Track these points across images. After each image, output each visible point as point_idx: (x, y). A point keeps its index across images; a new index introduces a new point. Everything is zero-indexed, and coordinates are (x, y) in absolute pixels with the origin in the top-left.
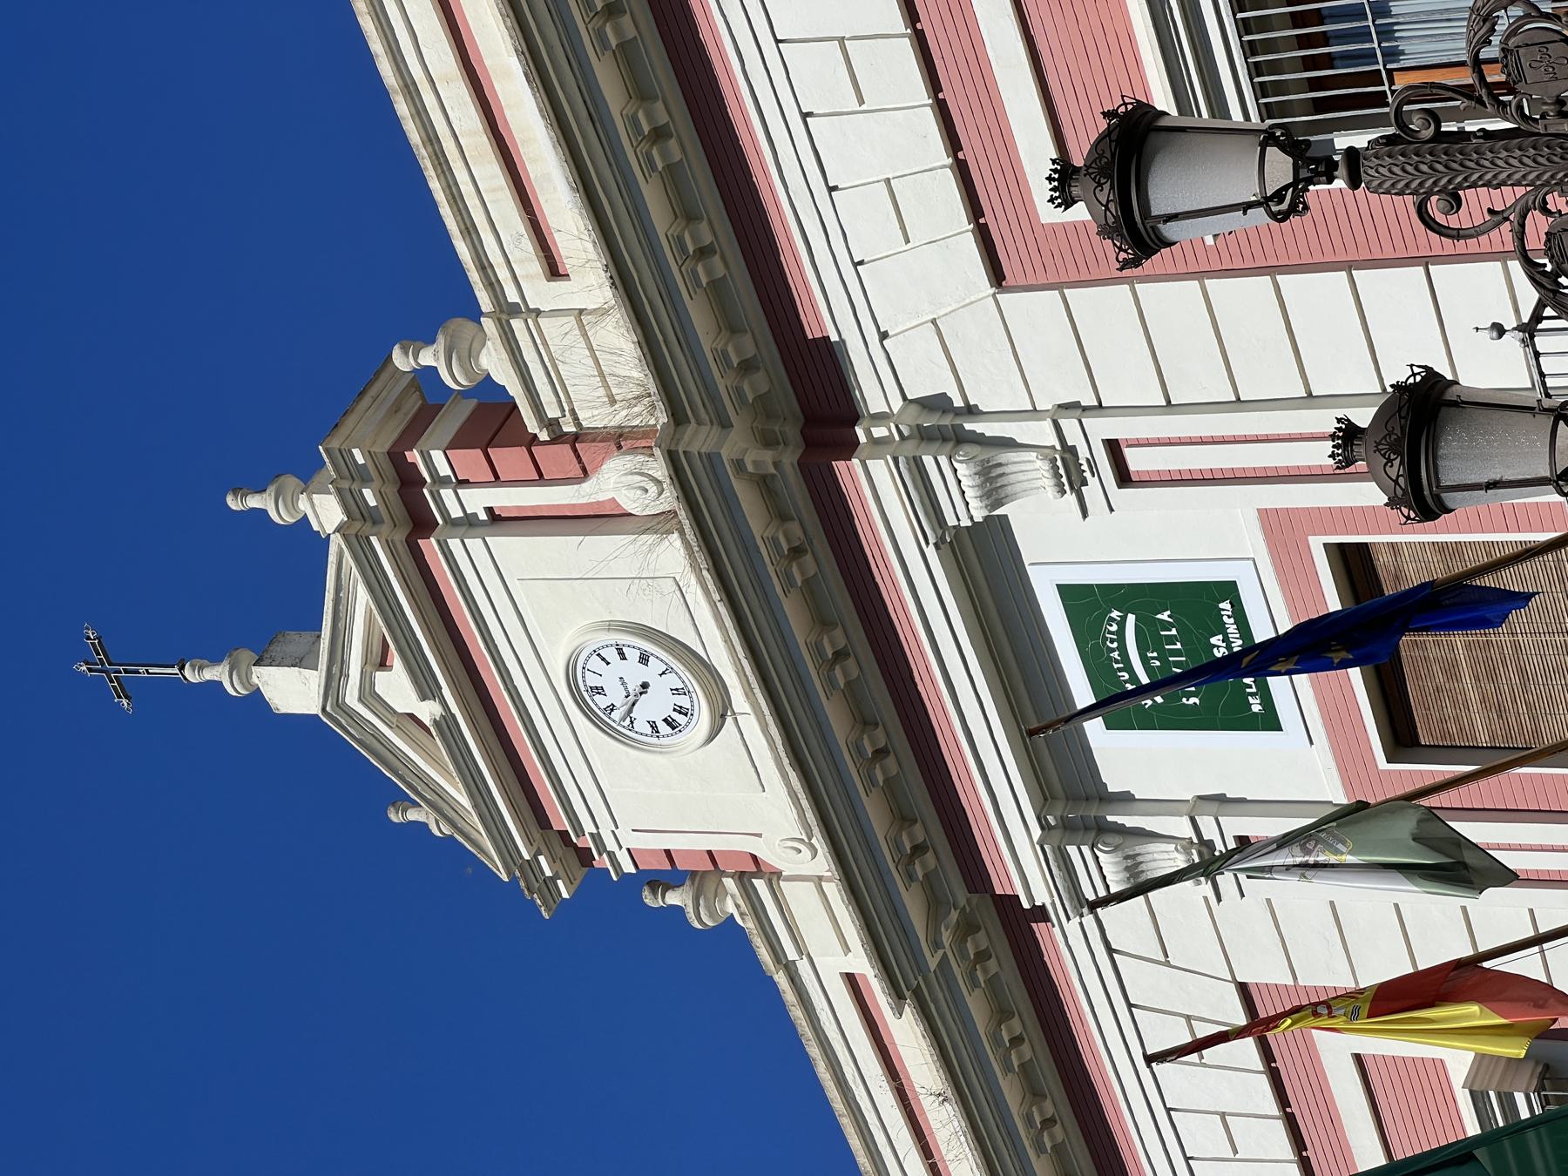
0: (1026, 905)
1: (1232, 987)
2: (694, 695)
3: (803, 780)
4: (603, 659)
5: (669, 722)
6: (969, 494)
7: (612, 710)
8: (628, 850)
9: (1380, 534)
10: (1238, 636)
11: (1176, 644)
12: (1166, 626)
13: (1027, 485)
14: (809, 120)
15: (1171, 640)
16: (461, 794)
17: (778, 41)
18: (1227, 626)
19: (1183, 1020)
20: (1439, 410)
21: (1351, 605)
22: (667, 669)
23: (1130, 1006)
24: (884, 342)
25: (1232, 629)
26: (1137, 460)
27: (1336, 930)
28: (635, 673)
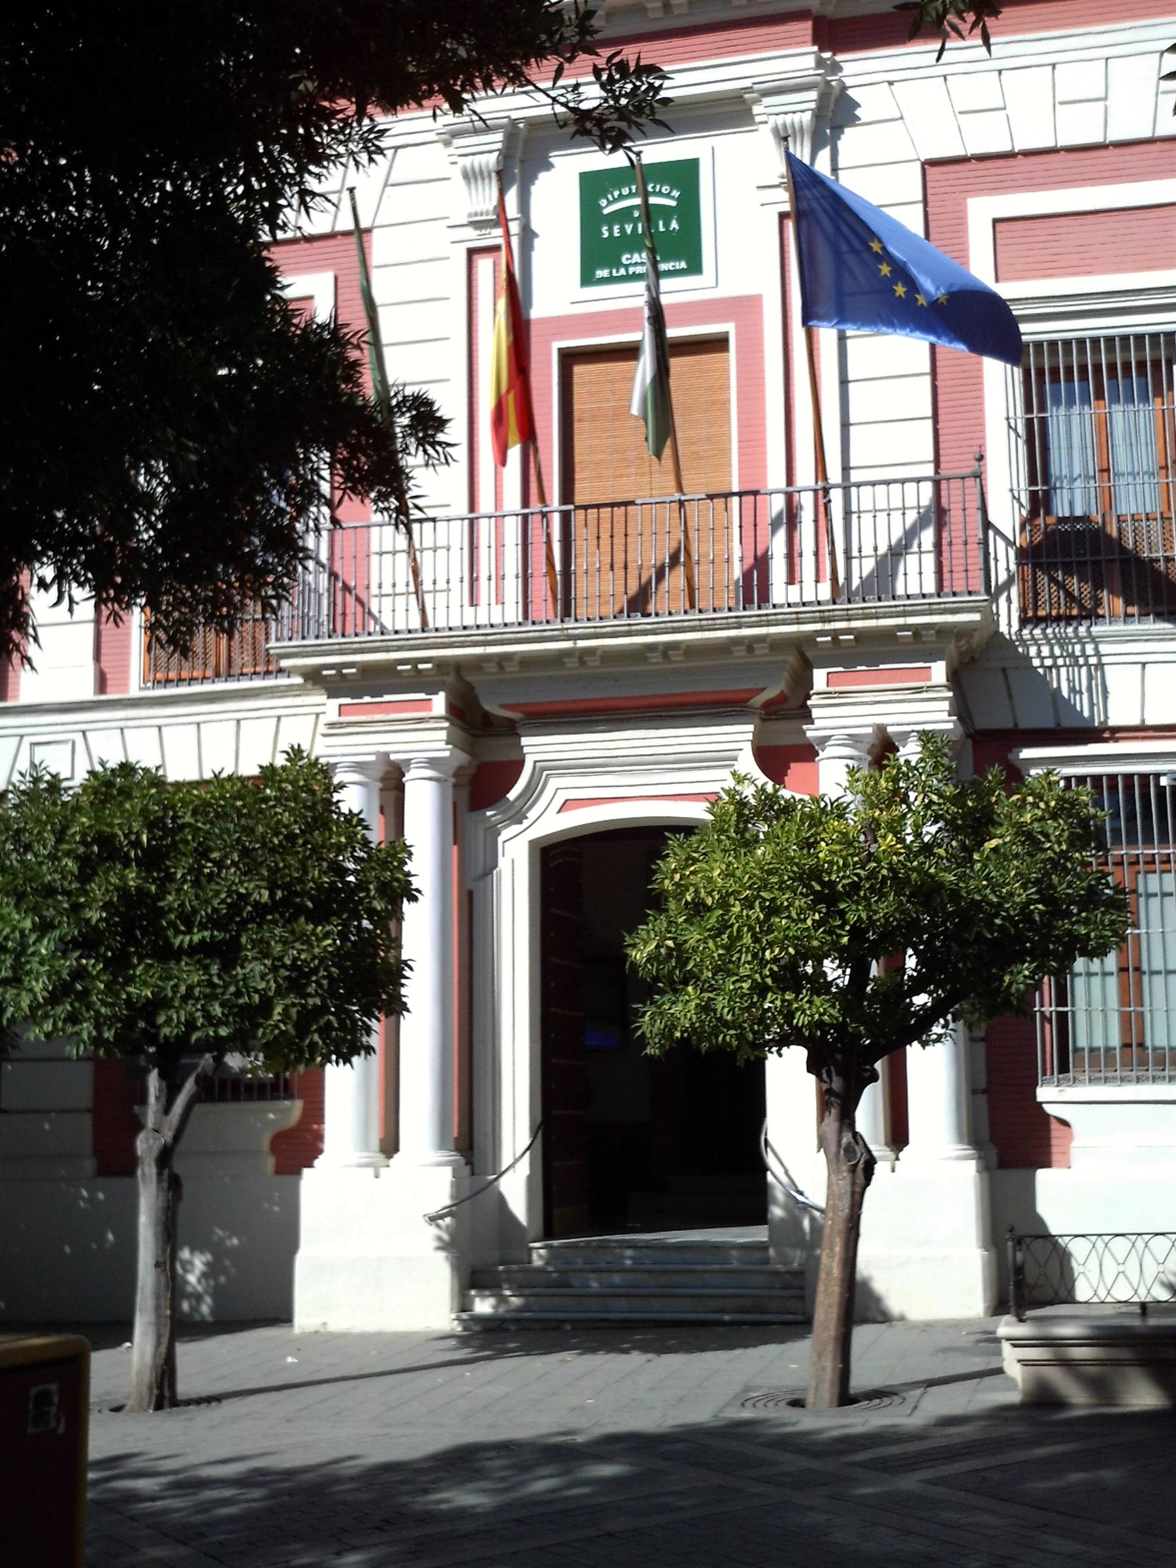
6: (788, 119)
13: (473, 189)
17: (1107, 59)
19: (388, 189)
20: (572, 369)
21: (1010, 756)
27: (325, 1386)
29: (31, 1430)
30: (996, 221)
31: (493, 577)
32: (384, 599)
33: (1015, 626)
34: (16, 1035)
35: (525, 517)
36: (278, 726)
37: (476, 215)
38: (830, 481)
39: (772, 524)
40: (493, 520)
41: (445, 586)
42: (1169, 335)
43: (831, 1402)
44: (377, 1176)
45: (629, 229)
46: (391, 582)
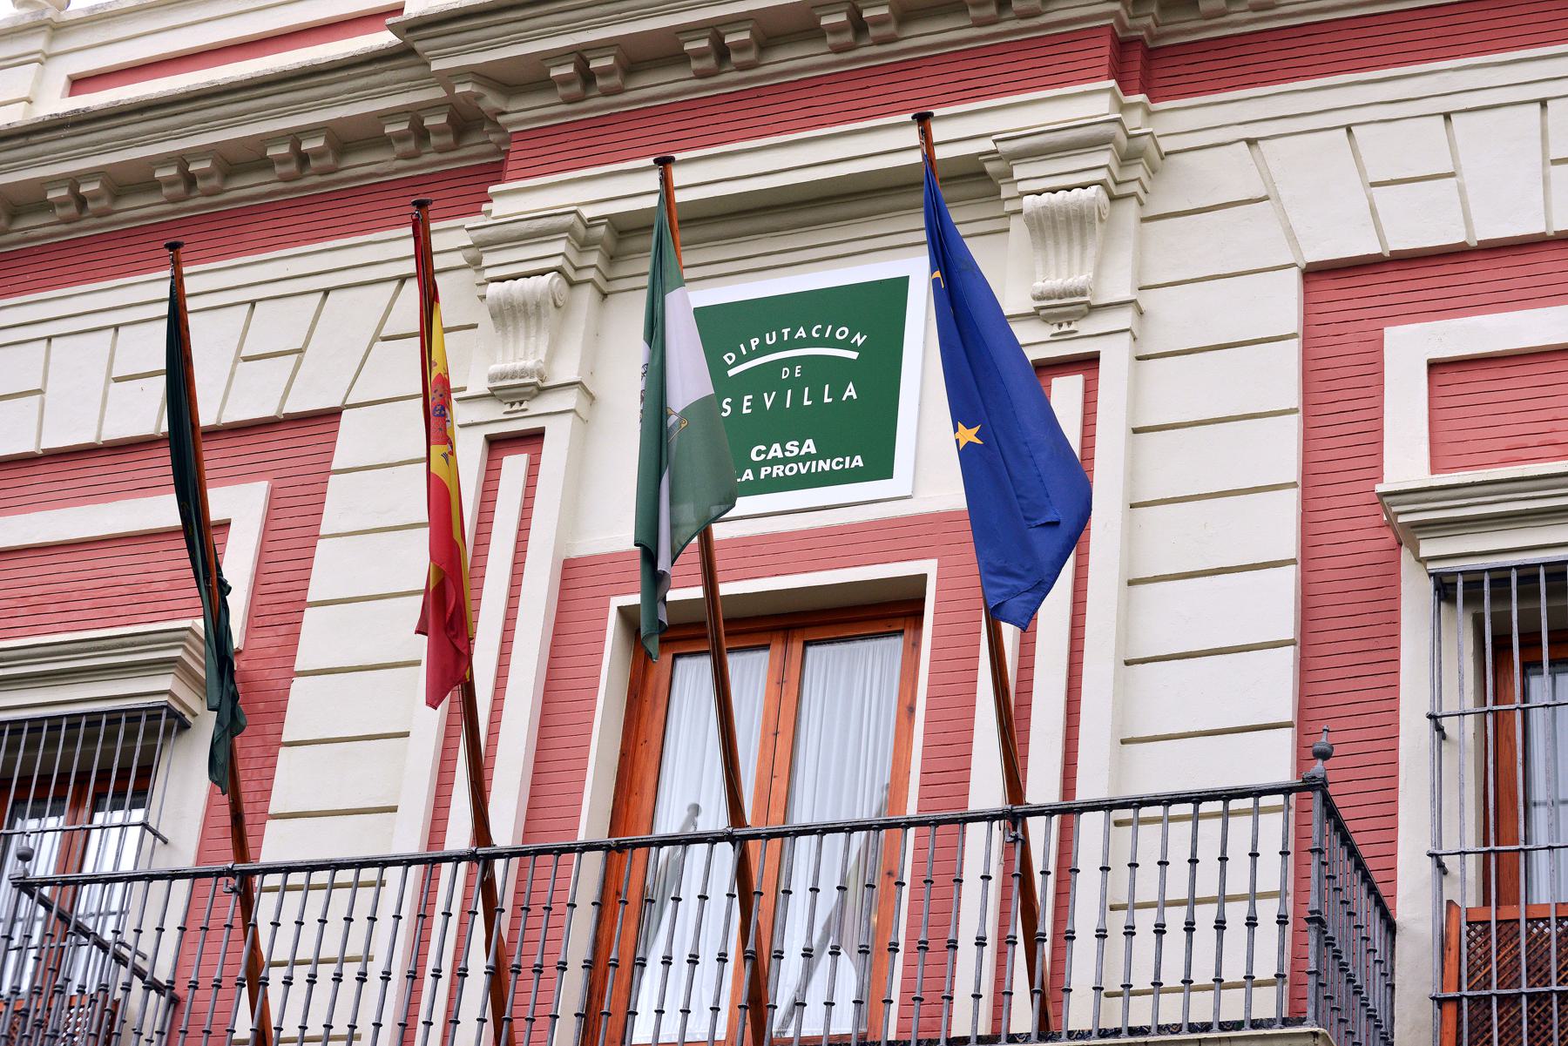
0: (491, 189)
1: (337, 403)
3: (462, 12)
10: (813, 470)
11: (828, 398)
12: (837, 392)
14: (249, 305)
15: (816, 396)
18: (828, 461)
25: (824, 465)
26: (514, 465)
29: (783, 377)
30: (1434, 366)
31: (991, 941)
32: (1154, 897)
34: (1003, 572)
35: (1486, 854)
36: (1157, 974)
37: (504, 376)
38: (1273, 1016)
40: (1056, 819)
41: (360, 952)
42: (1555, 571)
46: (688, 951)
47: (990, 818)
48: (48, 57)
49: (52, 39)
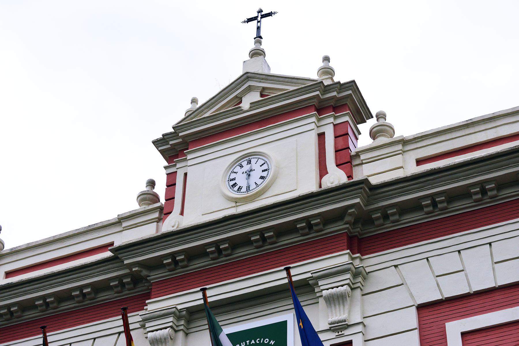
0: (147, 302)
2: (247, 193)
4: (263, 165)
5: (234, 185)
7: (241, 166)
8: (177, 172)
9: (446, 338)
16: (211, 114)
20: (204, 302)
22: (258, 185)
23: (95, 339)
24: (393, 267)
28: (255, 176)
33: (325, 293)
39: (328, 290)
43: (3, 278)
44: (254, 170)
45: (253, 342)
47: (205, 297)
48: (404, 152)
49: (403, 146)
